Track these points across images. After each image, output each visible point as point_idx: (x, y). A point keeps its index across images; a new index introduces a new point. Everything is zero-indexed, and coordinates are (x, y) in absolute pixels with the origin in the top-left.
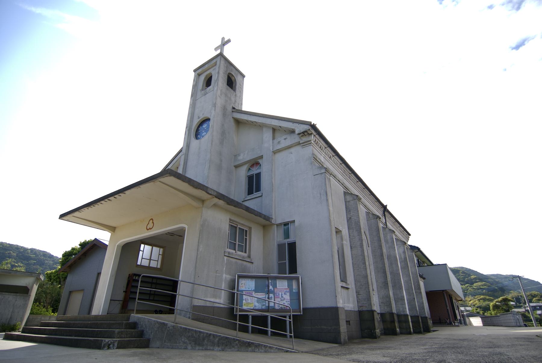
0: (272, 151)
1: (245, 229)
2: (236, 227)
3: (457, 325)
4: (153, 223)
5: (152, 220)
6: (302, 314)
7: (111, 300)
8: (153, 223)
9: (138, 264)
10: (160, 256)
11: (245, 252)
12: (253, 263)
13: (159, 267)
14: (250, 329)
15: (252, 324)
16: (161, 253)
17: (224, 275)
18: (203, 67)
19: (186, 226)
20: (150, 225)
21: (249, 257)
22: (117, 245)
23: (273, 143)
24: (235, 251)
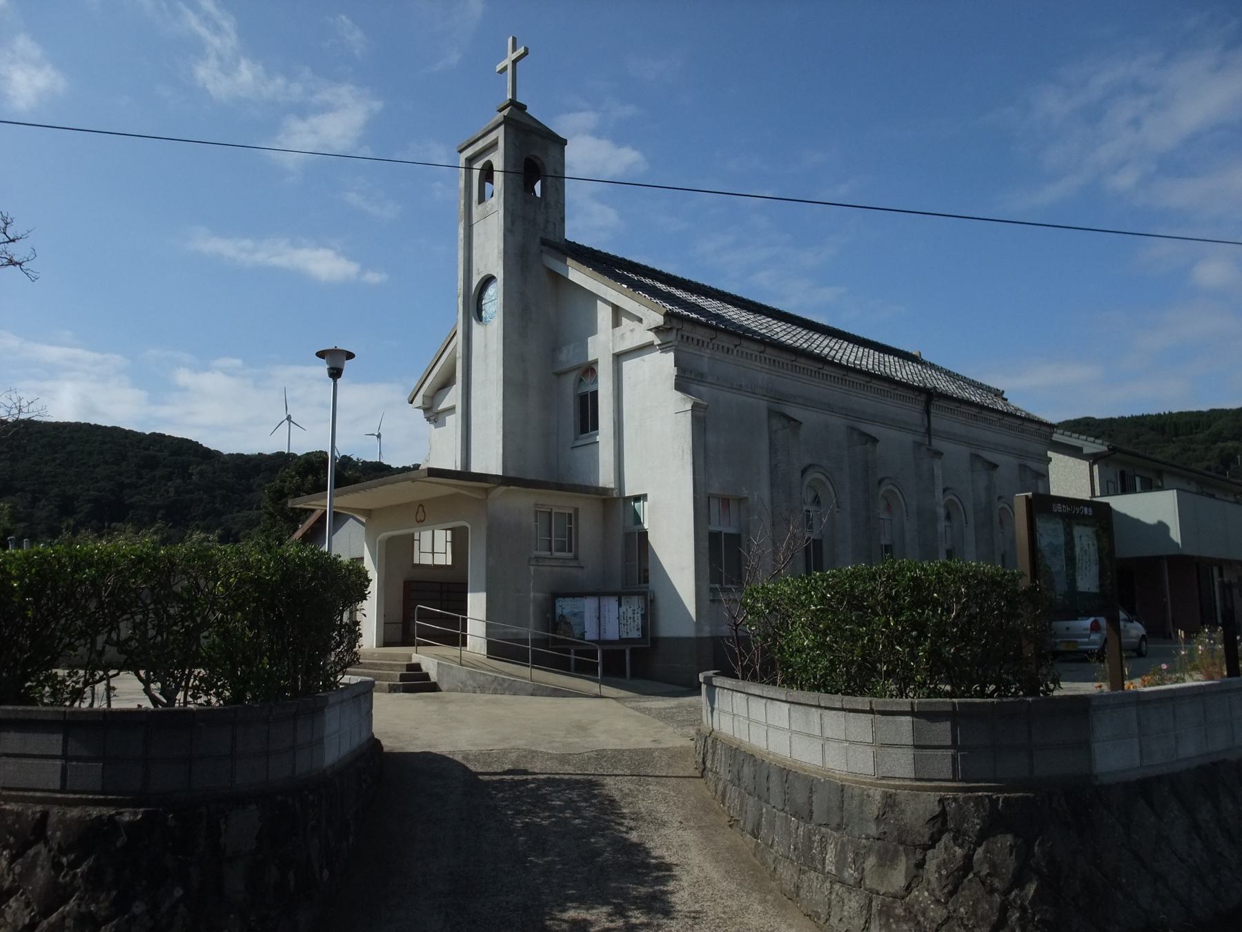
0: (612, 352)
1: (567, 512)
2: (550, 514)
3: (140, 676)
4: (424, 511)
5: (421, 507)
6: (649, 646)
7: (385, 623)
8: (424, 511)
9: (415, 562)
10: (449, 545)
11: (570, 551)
12: (583, 567)
13: (449, 563)
14: (572, 662)
15: (575, 655)
16: (449, 539)
17: (532, 594)
18: (473, 146)
19: (469, 526)
20: (420, 516)
21: (576, 558)
22: (378, 540)
23: (613, 335)
24: (549, 553)
